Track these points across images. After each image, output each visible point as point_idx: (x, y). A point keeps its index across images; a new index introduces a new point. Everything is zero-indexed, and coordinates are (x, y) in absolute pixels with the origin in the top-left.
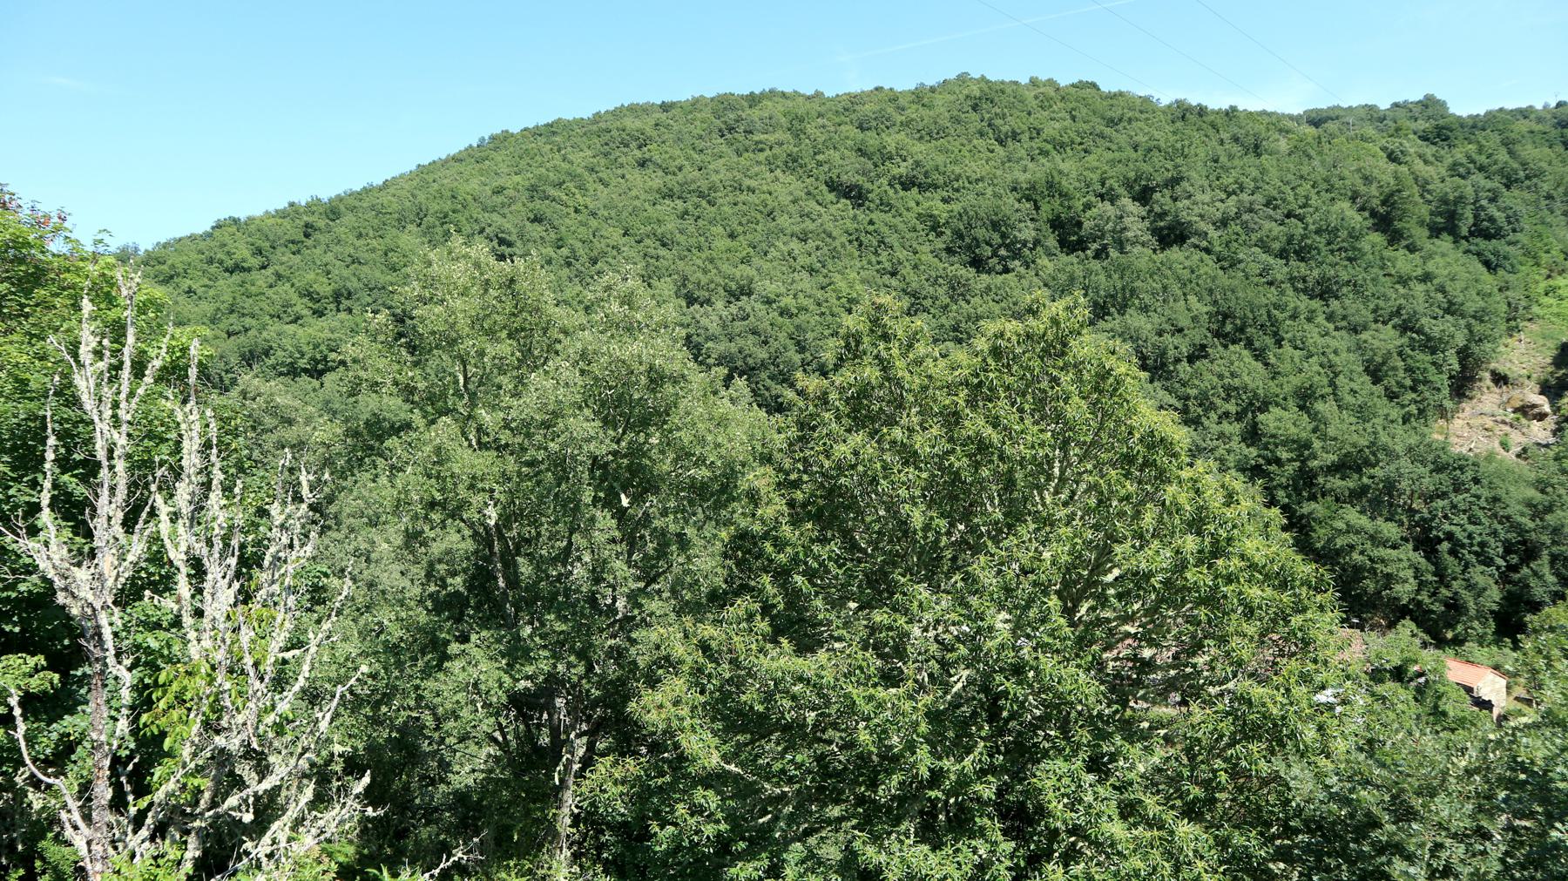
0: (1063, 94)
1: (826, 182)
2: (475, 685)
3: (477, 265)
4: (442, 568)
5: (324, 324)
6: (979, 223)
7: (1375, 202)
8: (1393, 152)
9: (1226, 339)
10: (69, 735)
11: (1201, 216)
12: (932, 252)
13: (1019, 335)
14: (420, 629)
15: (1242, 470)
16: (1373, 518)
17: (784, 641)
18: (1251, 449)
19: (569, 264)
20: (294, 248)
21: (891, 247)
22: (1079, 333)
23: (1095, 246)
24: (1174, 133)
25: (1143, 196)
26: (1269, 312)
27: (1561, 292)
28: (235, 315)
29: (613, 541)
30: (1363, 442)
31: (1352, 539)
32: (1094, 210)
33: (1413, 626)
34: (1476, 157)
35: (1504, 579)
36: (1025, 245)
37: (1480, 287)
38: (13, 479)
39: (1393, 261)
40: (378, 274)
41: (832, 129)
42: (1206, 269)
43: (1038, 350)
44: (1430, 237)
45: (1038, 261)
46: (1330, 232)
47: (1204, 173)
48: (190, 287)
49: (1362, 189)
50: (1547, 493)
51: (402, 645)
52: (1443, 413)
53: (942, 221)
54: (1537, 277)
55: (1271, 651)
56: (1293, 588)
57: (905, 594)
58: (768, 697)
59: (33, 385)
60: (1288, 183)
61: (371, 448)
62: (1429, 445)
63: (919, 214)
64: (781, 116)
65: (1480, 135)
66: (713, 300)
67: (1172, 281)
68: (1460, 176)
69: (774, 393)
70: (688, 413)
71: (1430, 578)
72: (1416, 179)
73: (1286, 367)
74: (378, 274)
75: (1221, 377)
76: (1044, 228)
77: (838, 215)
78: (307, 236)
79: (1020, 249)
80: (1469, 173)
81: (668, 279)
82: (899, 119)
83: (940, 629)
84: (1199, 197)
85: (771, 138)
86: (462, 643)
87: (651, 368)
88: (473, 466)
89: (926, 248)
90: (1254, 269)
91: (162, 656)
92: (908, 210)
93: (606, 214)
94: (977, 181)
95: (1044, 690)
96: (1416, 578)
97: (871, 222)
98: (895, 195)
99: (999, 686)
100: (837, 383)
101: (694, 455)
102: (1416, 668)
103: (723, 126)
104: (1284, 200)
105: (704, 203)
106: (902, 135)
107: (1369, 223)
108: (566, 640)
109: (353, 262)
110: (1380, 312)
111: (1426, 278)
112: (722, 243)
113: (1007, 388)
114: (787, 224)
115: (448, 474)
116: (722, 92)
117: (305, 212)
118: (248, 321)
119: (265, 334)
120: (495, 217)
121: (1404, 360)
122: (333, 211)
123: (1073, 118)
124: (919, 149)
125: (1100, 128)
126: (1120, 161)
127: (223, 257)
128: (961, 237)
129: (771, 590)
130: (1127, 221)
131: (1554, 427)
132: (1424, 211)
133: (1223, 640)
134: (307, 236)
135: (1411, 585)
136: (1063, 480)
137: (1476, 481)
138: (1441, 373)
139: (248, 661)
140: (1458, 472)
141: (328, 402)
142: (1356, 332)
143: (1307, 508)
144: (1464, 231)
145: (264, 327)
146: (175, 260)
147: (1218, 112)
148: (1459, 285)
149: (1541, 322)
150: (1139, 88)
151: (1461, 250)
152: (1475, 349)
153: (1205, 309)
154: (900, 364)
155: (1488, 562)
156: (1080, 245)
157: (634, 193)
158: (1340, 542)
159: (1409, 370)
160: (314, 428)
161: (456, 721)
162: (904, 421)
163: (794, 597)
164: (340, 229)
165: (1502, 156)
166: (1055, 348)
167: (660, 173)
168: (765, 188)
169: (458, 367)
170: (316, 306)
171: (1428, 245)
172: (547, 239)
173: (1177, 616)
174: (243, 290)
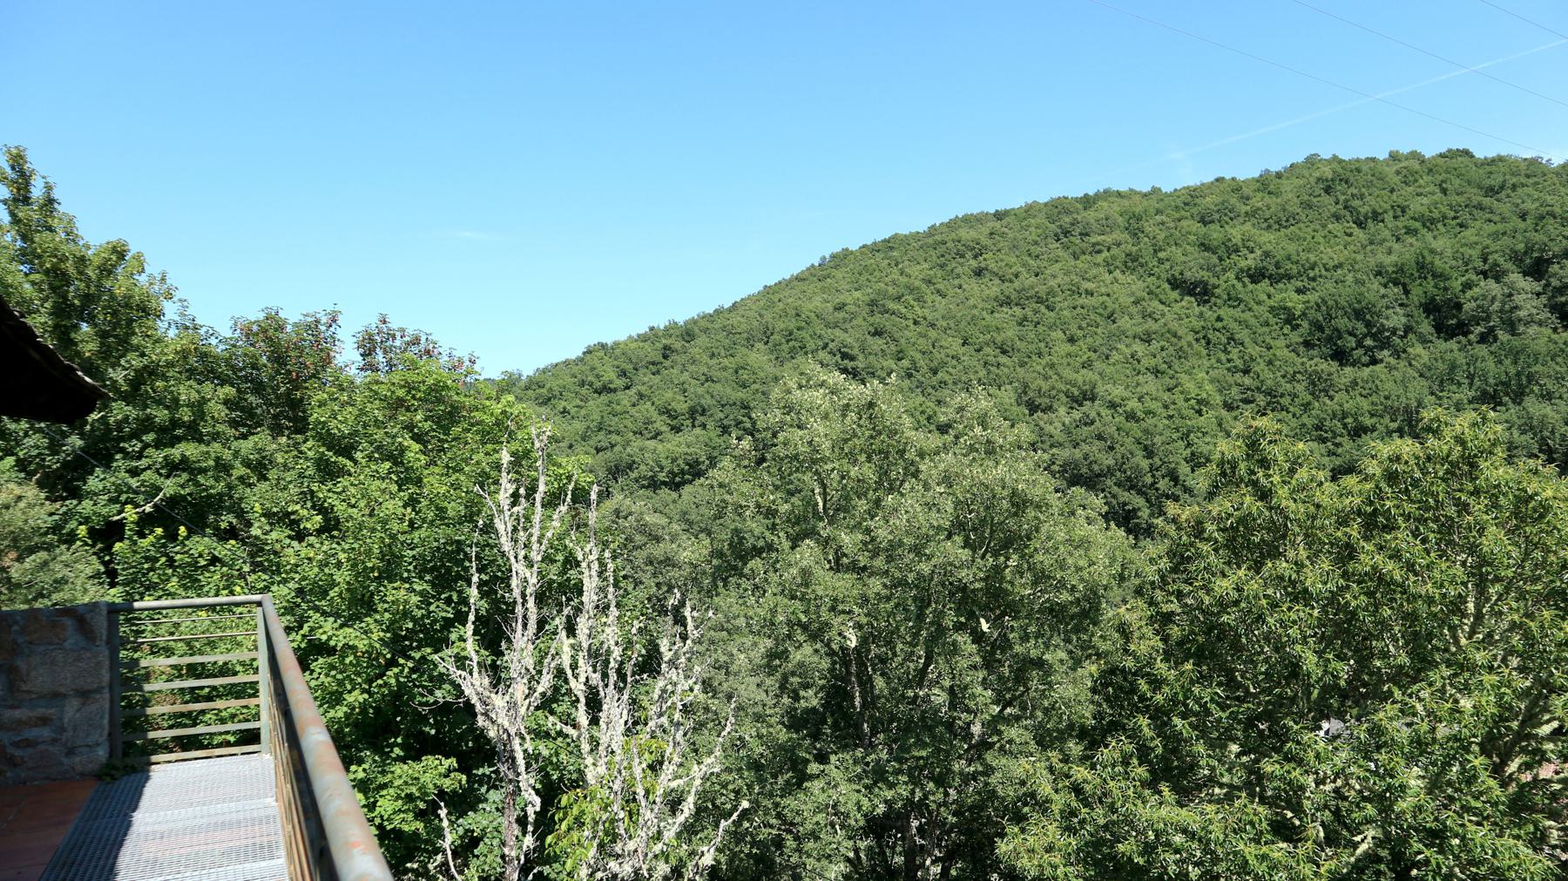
1: (1168, 281)
2: (834, 807)
4: (795, 680)
6: (1340, 313)
10: (473, 831)
12: (1288, 347)
13: (1417, 458)
14: (782, 747)
17: (1165, 788)
19: (910, 376)
20: (654, 369)
21: (1242, 344)
22: (1491, 453)
23: (1479, 329)
25: (1537, 269)
28: (603, 432)
29: (974, 667)
32: (1476, 290)
36: (1394, 333)
38: (433, 597)
41: (1172, 225)
43: (1441, 474)
45: (1410, 350)
51: (763, 761)
53: (1298, 313)
57: (1298, 743)
58: (1148, 849)
59: (451, 513)
61: (735, 568)
63: (1272, 308)
64: (1117, 216)
66: (1055, 406)
69: (1121, 500)
70: (1049, 538)
74: (729, 390)
76: (1416, 313)
77: (1184, 314)
78: (665, 357)
79: (1388, 338)
81: (1008, 387)
82: (1245, 209)
83: (1339, 783)
85: (1108, 239)
86: (820, 763)
87: (1014, 493)
88: (834, 589)
89: (1281, 342)
91: (551, 763)
92: (1259, 303)
93: (945, 324)
94: (1336, 268)
95: (1472, 863)
97: (1219, 319)
98: (1245, 290)
100: (1214, 513)
103: (1059, 231)
105: (1043, 309)
106: (1248, 226)
108: (925, 765)
109: (707, 381)
113: (1407, 517)
114: (1128, 326)
115: (813, 596)
116: (1055, 196)
117: (664, 335)
118: (614, 438)
119: (629, 450)
120: (838, 332)
122: (688, 333)
123: (1444, 191)
124: (1268, 239)
125: (1476, 199)
126: (1504, 234)
127: (593, 380)
128: (1321, 329)
129: (1148, 732)
130: (1518, 299)
134: (665, 357)
136: (1479, 616)
139: (641, 792)
141: (685, 513)
145: (628, 443)
146: (554, 384)
150: (1522, 150)
154: (1283, 492)
156: (1462, 329)
157: (972, 302)
161: (815, 841)
162: (1291, 554)
163: (1174, 742)
164: (695, 350)
167: (997, 281)
168: (1103, 290)
172: (888, 351)
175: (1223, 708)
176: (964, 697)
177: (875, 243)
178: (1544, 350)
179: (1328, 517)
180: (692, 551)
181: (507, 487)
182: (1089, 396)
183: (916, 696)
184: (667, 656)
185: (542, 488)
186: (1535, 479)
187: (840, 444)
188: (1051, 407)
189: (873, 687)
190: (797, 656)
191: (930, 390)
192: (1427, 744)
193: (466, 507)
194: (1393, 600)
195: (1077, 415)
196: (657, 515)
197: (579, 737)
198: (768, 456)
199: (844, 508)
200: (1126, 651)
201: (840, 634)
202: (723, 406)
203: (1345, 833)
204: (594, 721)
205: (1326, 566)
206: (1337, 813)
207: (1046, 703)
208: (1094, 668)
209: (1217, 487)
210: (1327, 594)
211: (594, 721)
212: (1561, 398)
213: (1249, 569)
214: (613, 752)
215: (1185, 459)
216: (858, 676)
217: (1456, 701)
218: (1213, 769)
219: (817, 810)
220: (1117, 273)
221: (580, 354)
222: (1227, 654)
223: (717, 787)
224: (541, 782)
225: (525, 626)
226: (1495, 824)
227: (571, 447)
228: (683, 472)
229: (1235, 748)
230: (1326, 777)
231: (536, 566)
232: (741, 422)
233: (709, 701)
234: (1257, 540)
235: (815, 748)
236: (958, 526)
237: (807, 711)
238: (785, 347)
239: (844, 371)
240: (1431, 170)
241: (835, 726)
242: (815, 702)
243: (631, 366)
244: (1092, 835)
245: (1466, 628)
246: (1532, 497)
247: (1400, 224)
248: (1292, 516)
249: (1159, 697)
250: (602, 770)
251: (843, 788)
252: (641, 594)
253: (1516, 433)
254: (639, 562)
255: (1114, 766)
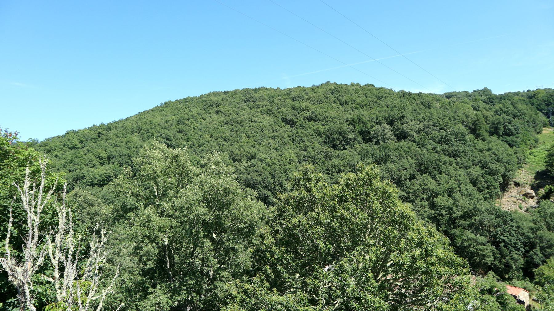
0: (362, 89)
2: (159, 304)
3: (163, 151)
4: (145, 258)
5: (104, 168)
6: (335, 133)
8: (475, 107)
9: (422, 172)
11: (411, 130)
12: (319, 143)
13: (355, 179)
15: (429, 218)
16: (476, 235)
17: (275, 290)
18: (432, 211)
19: (191, 147)
22: (376, 178)
23: (375, 140)
24: (401, 101)
25: (391, 123)
26: (436, 162)
27: (535, 154)
29: (211, 250)
30: (471, 207)
31: (469, 242)
32: (374, 128)
33: (493, 273)
35: (524, 255)
36: (351, 140)
39: (478, 144)
40: (123, 150)
41: (283, 100)
42: (414, 148)
43: (361, 184)
44: (489, 136)
45: (355, 146)
47: (412, 115)
48: (56, 154)
49: (466, 120)
50: (536, 224)
51: (131, 288)
52: (498, 197)
53: (322, 132)
54: (526, 149)
55: (448, 290)
56: (455, 266)
57: (317, 272)
60: (440, 118)
62: (494, 208)
65: (504, 101)
67: (402, 152)
68: (499, 115)
70: (237, 205)
71: (498, 256)
72: (484, 116)
73: (443, 181)
74: (123, 150)
75: (421, 185)
76: (357, 134)
77: (285, 131)
78: (99, 136)
79: (349, 142)
80: (501, 114)
81: (226, 153)
83: (330, 284)
84: (410, 123)
85: (262, 104)
87: (225, 188)
89: (317, 141)
90: (430, 147)
91: (43, 295)
92: (310, 128)
93: (204, 130)
96: (493, 256)
97: (297, 133)
98: (306, 123)
99: (352, 305)
100: (292, 196)
101: (239, 219)
102: (496, 289)
104: (439, 124)
105: (239, 126)
106: (307, 103)
107: (469, 131)
109: (115, 146)
110: (474, 162)
111: (489, 150)
112: (245, 140)
113: (352, 198)
115: (151, 226)
118: (77, 167)
119: (82, 171)
120: (166, 130)
121: (483, 178)
122: (108, 128)
123: (366, 97)
124: (314, 107)
126: (383, 111)
127: (69, 144)
128: (329, 138)
129: (269, 271)
130: (386, 132)
131: (537, 201)
132: (487, 127)
133: (431, 287)
134: (99, 136)
135: (492, 258)
136: (372, 229)
137: (512, 220)
138: (497, 182)
139: (80, 302)
140: (505, 218)
141: (104, 196)
142: (467, 169)
143: (453, 231)
144: (501, 133)
145: (82, 169)
146: (52, 145)
147: (415, 94)
148: (501, 152)
149: (529, 164)
152: (508, 174)
153: (414, 162)
154: (314, 189)
155: (518, 250)
156: (370, 140)
157: (214, 122)
158: (466, 244)
159: (486, 182)
160: (101, 208)
162: (316, 210)
163: (278, 274)
165: (511, 108)
166: (369, 182)
167: (223, 116)
168: (260, 121)
169: (152, 184)
171: (489, 138)
172: (184, 138)
173: (415, 278)
174: (75, 155)
175: (294, 261)
176: (207, 261)
177: (181, 100)
178: (392, 148)
179: (328, 198)
180: (105, 210)
181: (27, 183)
182: (253, 157)
183: (190, 262)
184: (93, 248)
185: (43, 183)
186: (388, 186)
187: (164, 171)
188: (241, 160)
189: (174, 259)
190: (146, 249)
191: (198, 153)
192: (356, 270)
193: (10, 192)
194: (347, 224)
195: (249, 163)
196: (92, 196)
197: (54, 282)
198: (137, 175)
199: (165, 194)
200: (262, 243)
201: (162, 240)
202: (121, 156)
203: (332, 301)
204: (62, 276)
205: (327, 214)
206: (330, 295)
207: (236, 263)
208: (252, 250)
209: (293, 187)
210: (327, 223)
211: (62, 276)
212: (397, 163)
213: (303, 215)
214: (69, 287)
215: (285, 179)
216: (168, 256)
217: (365, 256)
218: (290, 282)
219: (152, 306)
220: (265, 116)
221: (64, 134)
222: (296, 244)
223: (113, 300)
224: (38, 303)
225: (33, 238)
226: (375, 294)
227: (58, 169)
228: (104, 180)
229: (298, 275)
230: (326, 283)
231: (39, 215)
232: (128, 162)
233: (111, 267)
234: (306, 205)
235: (152, 283)
236: (204, 200)
237: (149, 269)
238: (146, 135)
239: (168, 144)
240: (363, 90)
241: (159, 274)
242: (152, 266)
243: (85, 139)
244: (250, 308)
245: (368, 233)
246: (387, 192)
247: (353, 106)
248: (317, 197)
249: (273, 259)
250: (64, 295)
251: (162, 297)
252: (85, 226)
253: (385, 173)
254: (84, 214)
255: (258, 283)
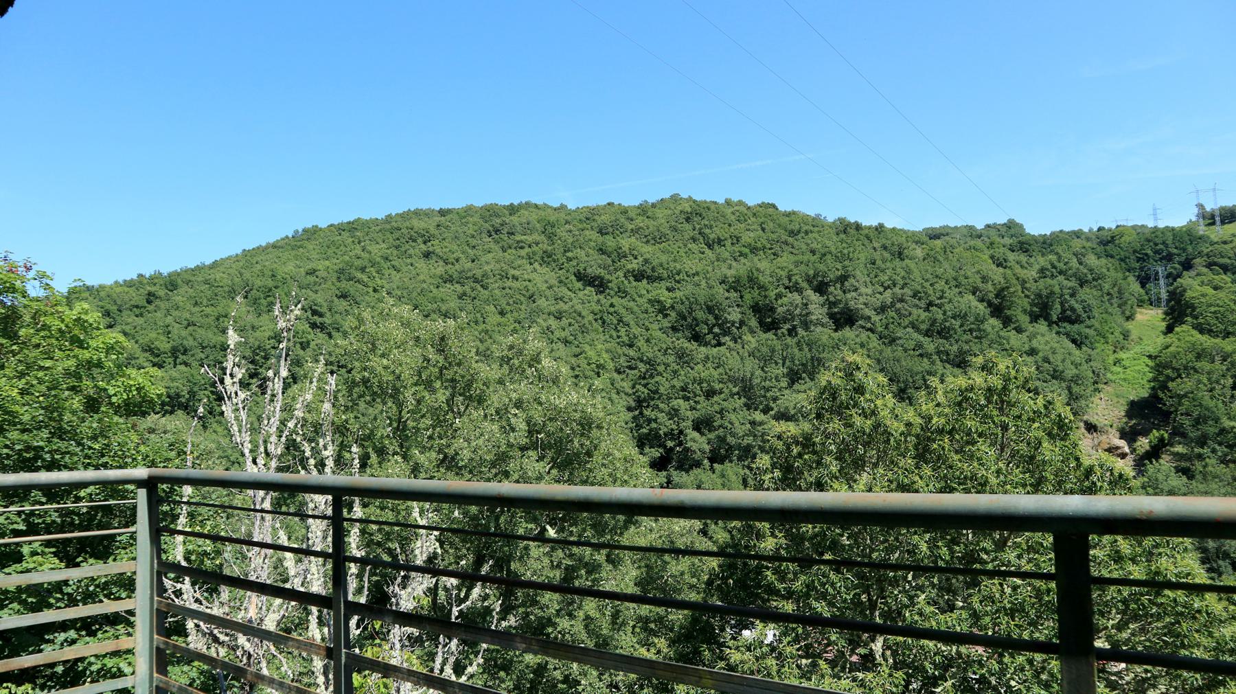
1: (575, 274)
7: (991, 296)
11: (865, 304)
12: (660, 329)
20: (137, 311)
23: (788, 326)
25: (821, 288)
34: (1058, 264)
36: (733, 325)
37: (1072, 359)
40: (210, 335)
41: (577, 233)
44: (1031, 322)
45: (744, 337)
46: (963, 317)
53: (668, 305)
60: (927, 281)
63: (649, 300)
74: (210, 335)
78: (149, 302)
79: (729, 328)
82: (631, 227)
84: (863, 290)
85: (529, 239)
89: (655, 326)
90: (912, 344)
93: (399, 293)
97: (612, 305)
98: (631, 285)
103: (491, 229)
106: (633, 239)
111: (1032, 352)
112: (494, 318)
117: (148, 283)
122: (172, 283)
123: (763, 230)
124: (647, 250)
125: (784, 237)
128: (684, 318)
134: (149, 302)
147: (870, 228)
148: (1059, 357)
150: (809, 209)
151: (1054, 331)
157: (419, 278)
164: (178, 298)
167: (441, 263)
168: (526, 277)
170: (156, 360)
